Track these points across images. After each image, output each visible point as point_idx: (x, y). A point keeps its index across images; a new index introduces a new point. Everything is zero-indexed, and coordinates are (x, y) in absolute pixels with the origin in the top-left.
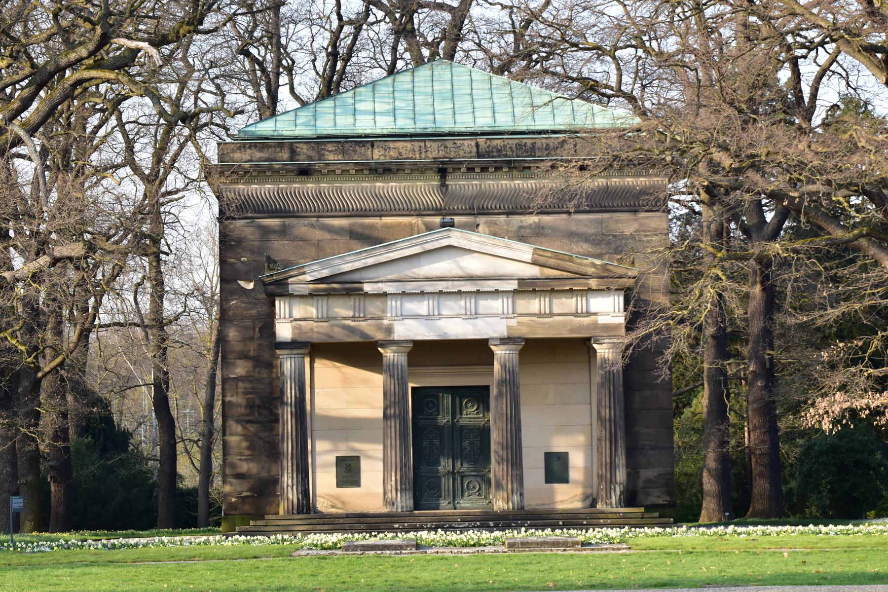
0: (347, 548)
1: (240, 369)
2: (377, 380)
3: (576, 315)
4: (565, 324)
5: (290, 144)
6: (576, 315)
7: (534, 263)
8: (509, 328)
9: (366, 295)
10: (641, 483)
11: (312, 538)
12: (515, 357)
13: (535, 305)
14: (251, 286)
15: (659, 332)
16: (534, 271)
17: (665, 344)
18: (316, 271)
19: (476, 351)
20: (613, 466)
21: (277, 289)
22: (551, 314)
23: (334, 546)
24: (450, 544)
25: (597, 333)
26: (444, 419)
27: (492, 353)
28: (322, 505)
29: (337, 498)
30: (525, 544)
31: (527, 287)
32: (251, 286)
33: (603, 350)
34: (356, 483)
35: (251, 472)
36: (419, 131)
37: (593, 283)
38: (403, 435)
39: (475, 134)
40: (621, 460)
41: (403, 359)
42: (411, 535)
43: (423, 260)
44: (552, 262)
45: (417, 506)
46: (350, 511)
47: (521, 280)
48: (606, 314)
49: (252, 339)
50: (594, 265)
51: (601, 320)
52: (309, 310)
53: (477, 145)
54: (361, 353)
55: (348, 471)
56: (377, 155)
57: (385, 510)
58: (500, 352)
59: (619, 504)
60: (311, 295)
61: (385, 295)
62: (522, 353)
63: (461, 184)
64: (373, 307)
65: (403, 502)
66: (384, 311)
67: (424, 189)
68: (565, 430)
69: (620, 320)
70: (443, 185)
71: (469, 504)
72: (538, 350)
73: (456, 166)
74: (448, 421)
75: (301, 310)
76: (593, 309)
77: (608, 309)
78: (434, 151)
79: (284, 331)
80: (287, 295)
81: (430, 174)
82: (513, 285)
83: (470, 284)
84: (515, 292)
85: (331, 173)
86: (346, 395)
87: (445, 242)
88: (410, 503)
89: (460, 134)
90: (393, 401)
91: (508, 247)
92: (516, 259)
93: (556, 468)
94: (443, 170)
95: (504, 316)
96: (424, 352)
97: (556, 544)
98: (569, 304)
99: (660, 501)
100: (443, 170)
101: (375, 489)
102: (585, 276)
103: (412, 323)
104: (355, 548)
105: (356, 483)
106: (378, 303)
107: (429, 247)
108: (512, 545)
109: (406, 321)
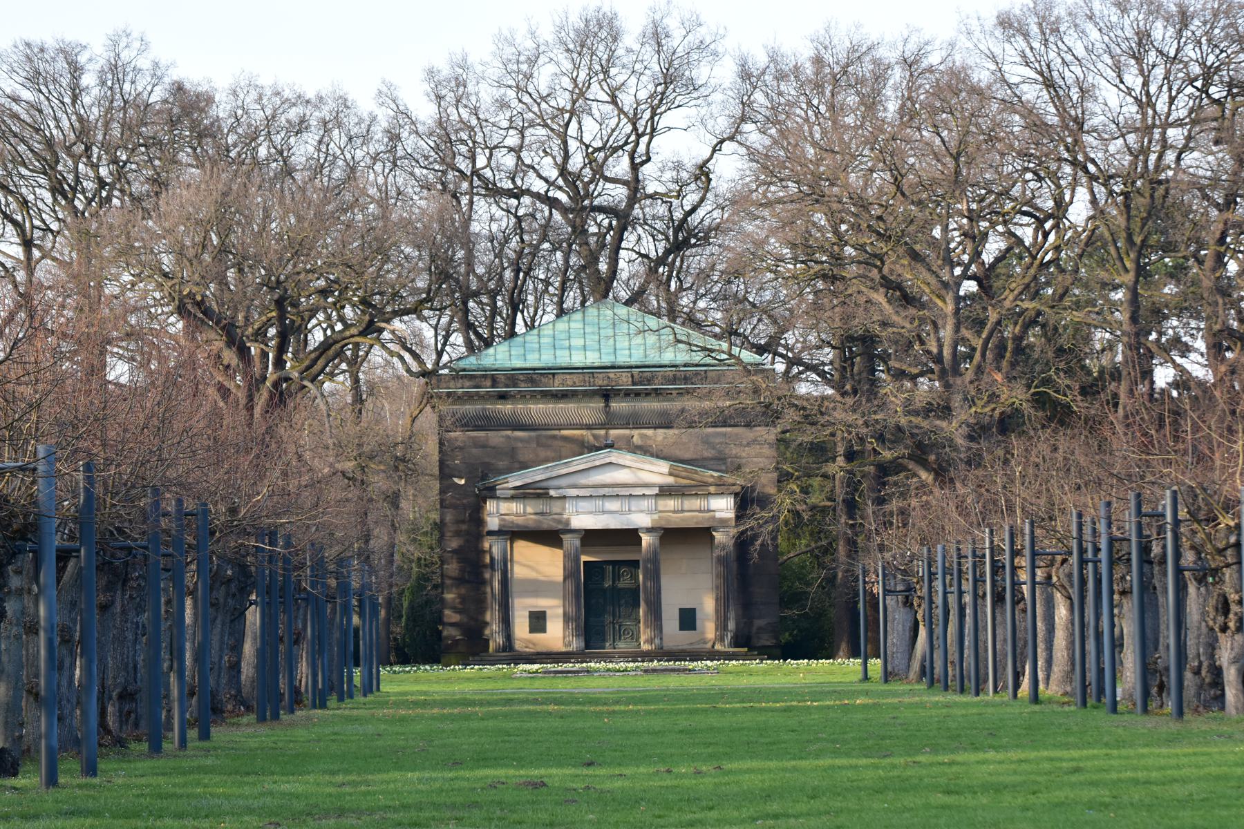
0: (545, 673)
1: (454, 544)
2: (559, 553)
3: (700, 511)
4: (693, 517)
5: (492, 376)
6: (700, 511)
7: (670, 474)
8: (653, 520)
9: (551, 497)
10: (754, 629)
11: (522, 667)
12: (657, 542)
13: (671, 504)
14: (463, 482)
15: (752, 528)
16: (671, 480)
17: (755, 537)
18: (515, 480)
19: (630, 536)
20: (726, 619)
21: (490, 492)
22: (683, 511)
23: (536, 672)
24: (609, 670)
25: (715, 524)
26: (608, 584)
27: (640, 539)
28: (518, 646)
29: (530, 641)
30: (654, 670)
31: (665, 492)
32: (463, 482)
33: (719, 536)
34: (543, 630)
35: (447, 616)
36: (589, 364)
37: (712, 489)
38: (577, 597)
39: (631, 367)
40: (732, 615)
41: (577, 542)
42: (584, 665)
43: (592, 472)
44: (684, 474)
45: (587, 647)
46: (539, 650)
47: (661, 487)
48: (722, 510)
49: (463, 522)
50: (712, 476)
51: (718, 515)
52: (514, 507)
53: (632, 376)
54: (549, 536)
55: (538, 621)
56: (557, 386)
57: (564, 649)
58: (646, 539)
59: (730, 646)
60: (513, 498)
61: (565, 497)
62: (662, 539)
63: (617, 405)
64: (556, 507)
65: (576, 644)
66: (564, 509)
67: (590, 411)
68: (693, 589)
69: (731, 515)
70: (607, 406)
71: (622, 646)
72: (673, 536)
73: (617, 393)
74: (610, 586)
75: (505, 507)
76: (712, 507)
77: (723, 507)
78: (600, 381)
79: (493, 523)
80: (494, 497)
81: (597, 398)
82: (656, 491)
83: (623, 490)
84: (657, 495)
85: (523, 396)
86: (539, 565)
87: (608, 460)
88: (582, 644)
89: (620, 367)
90: (570, 574)
91: (651, 463)
92: (657, 472)
93: (688, 619)
94: (606, 395)
95: (650, 512)
96: (591, 537)
97: (673, 670)
98: (696, 503)
99: (769, 643)
100: (606, 395)
101: (556, 635)
102: (707, 484)
103: (584, 518)
104: (550, 672)
105: (543, 630)
106: (559, 503)
107: (597, 463)
108: (646, 671)
109: (581, 516)
